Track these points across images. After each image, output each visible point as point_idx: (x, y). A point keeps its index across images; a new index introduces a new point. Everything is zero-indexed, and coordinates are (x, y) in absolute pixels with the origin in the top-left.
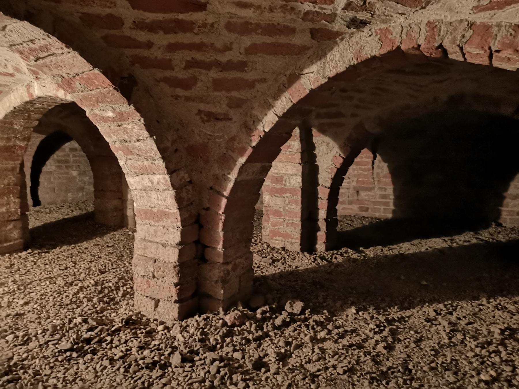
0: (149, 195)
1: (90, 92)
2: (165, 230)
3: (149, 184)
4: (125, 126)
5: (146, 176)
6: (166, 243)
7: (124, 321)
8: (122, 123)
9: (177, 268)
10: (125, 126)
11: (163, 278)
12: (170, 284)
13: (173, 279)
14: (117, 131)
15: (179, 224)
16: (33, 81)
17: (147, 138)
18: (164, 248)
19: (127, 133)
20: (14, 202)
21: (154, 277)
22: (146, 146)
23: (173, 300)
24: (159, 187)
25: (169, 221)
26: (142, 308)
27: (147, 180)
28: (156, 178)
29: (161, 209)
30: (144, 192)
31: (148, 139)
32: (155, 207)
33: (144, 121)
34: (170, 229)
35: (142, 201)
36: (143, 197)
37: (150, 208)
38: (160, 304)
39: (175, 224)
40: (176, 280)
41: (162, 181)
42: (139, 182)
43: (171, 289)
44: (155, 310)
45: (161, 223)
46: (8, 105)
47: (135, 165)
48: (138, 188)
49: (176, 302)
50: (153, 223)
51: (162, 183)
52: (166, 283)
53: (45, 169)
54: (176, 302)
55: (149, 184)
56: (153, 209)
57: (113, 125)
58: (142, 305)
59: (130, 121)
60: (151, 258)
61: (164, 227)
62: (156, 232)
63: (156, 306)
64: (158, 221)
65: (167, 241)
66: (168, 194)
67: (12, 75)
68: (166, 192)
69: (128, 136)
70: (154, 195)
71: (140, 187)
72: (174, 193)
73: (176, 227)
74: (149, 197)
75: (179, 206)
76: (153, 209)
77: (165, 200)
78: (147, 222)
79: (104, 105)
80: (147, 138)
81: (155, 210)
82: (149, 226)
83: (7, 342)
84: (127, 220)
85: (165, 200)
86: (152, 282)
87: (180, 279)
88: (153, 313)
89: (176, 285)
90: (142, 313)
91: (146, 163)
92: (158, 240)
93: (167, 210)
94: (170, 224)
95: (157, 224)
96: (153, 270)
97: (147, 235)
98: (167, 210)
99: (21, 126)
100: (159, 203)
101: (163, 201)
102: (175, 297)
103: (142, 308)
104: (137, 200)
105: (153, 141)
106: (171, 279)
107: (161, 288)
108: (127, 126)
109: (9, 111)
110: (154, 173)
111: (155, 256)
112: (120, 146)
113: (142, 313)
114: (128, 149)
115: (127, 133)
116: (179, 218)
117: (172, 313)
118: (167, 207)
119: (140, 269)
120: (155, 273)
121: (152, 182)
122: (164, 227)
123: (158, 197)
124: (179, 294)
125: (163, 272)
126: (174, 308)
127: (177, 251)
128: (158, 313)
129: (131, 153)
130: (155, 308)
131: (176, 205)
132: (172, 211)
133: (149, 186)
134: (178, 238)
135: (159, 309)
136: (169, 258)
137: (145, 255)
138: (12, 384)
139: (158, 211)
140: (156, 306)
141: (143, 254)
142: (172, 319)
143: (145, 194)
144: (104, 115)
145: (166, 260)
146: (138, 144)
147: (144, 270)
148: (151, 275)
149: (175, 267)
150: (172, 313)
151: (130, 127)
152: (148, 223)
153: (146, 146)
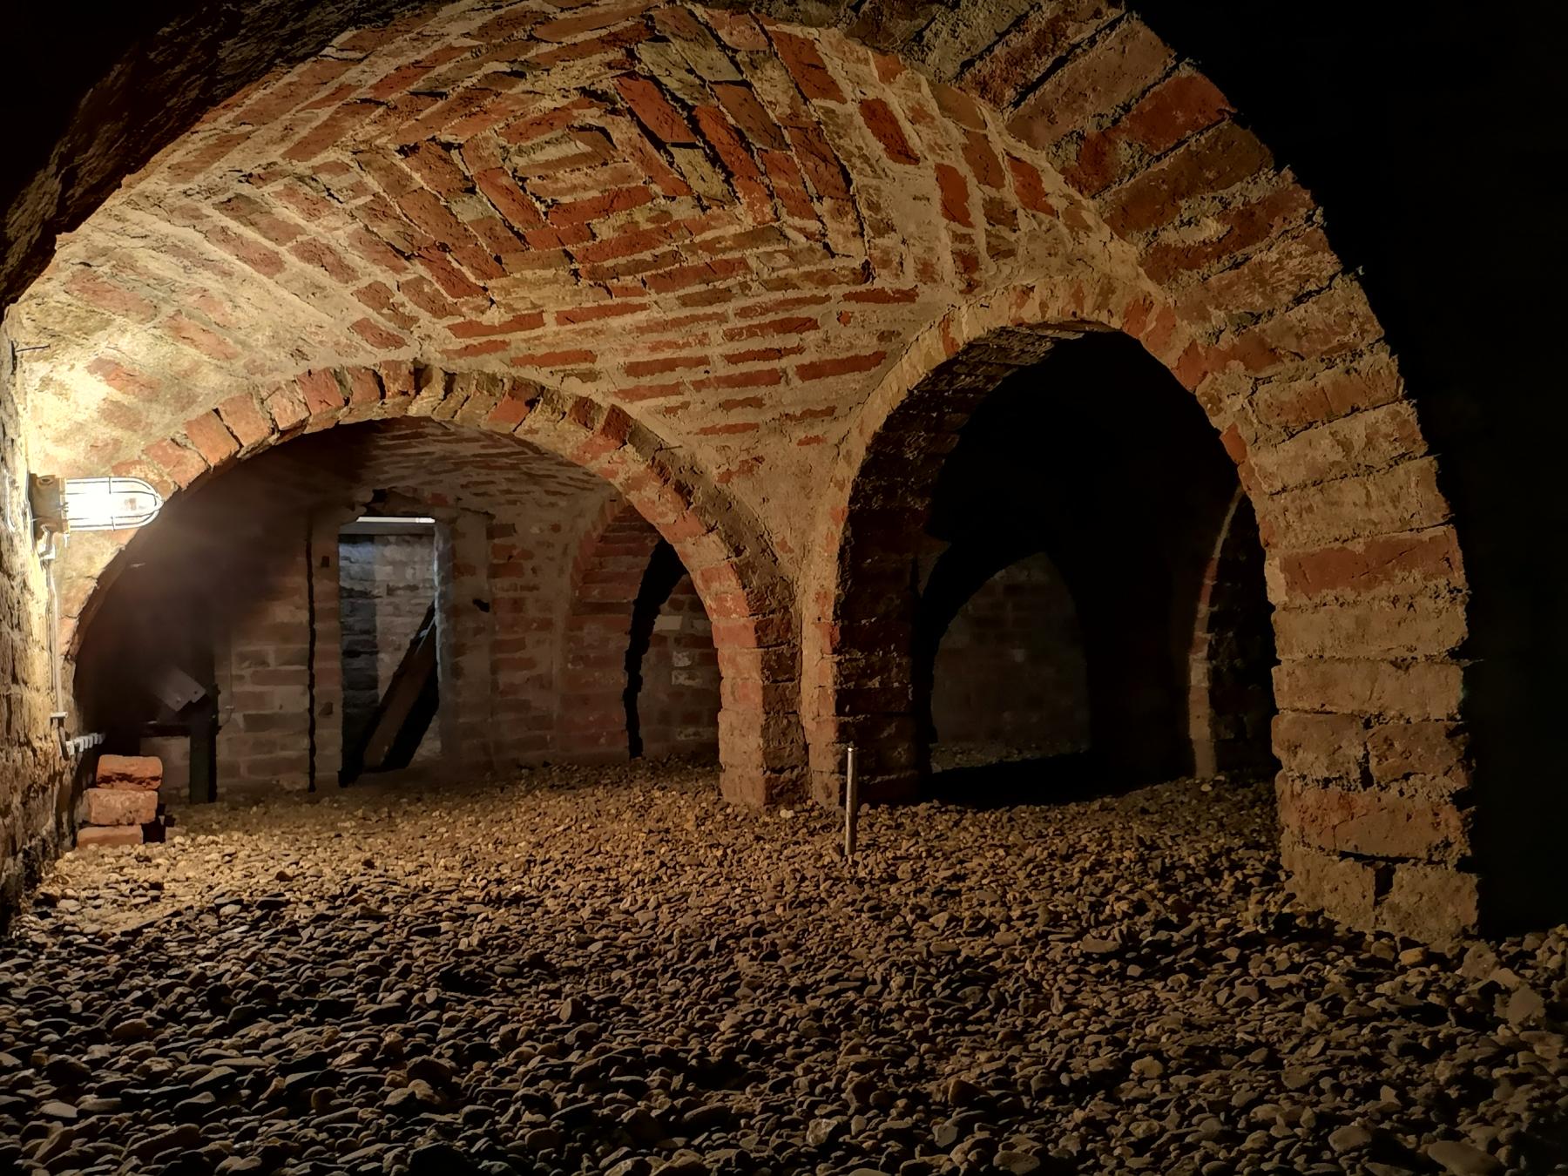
0: (1335, 496)
1: (1155, 168)
2: (1401, 609)
3: (1337, 455)
4: (1256, 258)
5: (1325, 430)
6: (1409, 655)
7: (1271, 920)
8: (1248, 250)
9: (1460, 738)
10: (1256, 258)
11: (1406, 777)
12: (1434, 797)
13: (1446, 780)
14: (1230, 286)
15: (1459, 577)
16: (959, 301)
17: (1332, 278)
18: (1401, 672)
19: (1263, 283)
20: (899, 665)
21: (1367, 780)
22: (1329, 310)
23: (1452, 860)
24: (1375, 458)
25: (1417, 573)
26: (1328, 897)
27: (1326, 442)
28: (1356, 428)
29: (1381, 539)
30: (1312, 490)
31: (1338, 280)
32: (1356, 536)
33: (1325, 216)
34: (1424, 602)
35: (1308, 527)
36: (1310, 509)
37: (1337, 545)
38: (1401, 874)
39: (1442, 582)
40: (1458, 782)
41: (1384, 429)
42: (1296, 457)
43: (1442, 816)
44: (1377, 903)
45: (1383, 589)
46: (895, 389)
47: (1285, 397)
48: (1291, 483)
49: (1463, 865)
50: (1350, 595)
51: (1387, 436)
52: (1420, 799)
53: (946, 642)
54: (1463, 865)
55: (1337, 455)
56: (1349, 545)
57: (1217, 267)
58: (1327, 888)
59: (1274, 233)
60: (1352, 717)
61: (1395, 601)
62: (1362, 623)
63: (1384, 884)
64: (1369, 586)
65: (1410, 650)
66: (1407, 473)
67: (909, 296)
68: (1400, 470)
69: (1263, 294)
70: (1352, 492)
71: (1300, 474)
72: (1435, 463)
73: (1444, 592)
74: (1333, 504)
75: (1452, 508)
76: (1349, 545)
77: (1395, 500)
78: (1329, 595)
79: (1193, 202)
80: (1332, 278)
81: (1358, 547)
82: (1336, 607)
83: (933, 927)
84: (1192, 754)
85: (1395, 500)
86: (1363, 798)
87: (1475, 778)
88: (1372, 915)
89: (1459, 800)
90: (1326, 914)
91: (1325, 378)
92: (1374, 650)
93: (1407, 535)
94: (1420, 585)
95: (1366, 596)
96: (1362, 753)
97: (1329, 643)
98: (1407, 535)
99: (921, 450)
100: (1374, 516)
101: (1389, 506)
102: (1461, 848)
103: (1328, 897)
104: (1288, 526)
105: (1356, 284)
106: (1441, 780)
107: (1402, 817)
108: (1264, 256)
109: (896, 404)
110: (1355, 410)
111: (1366, 707)
112: (1236, 341)
113: (1326, 914)
114: (1261, 342)
115: (1263, 283)
116: (1458, 556)
117: (1451, 909)
118: (1405, 524)
119: (1311, 757)
120: (1373, 763)
121: (1346, 446)
122: (1395, 601)
123: (1368, 494)
124: (1475, 833)
125: (1406, 754)
126: (1458, 889)
127: (1455, 675)
128: (1394, 909)
129: (1273, 355)
130: (1377, 894)
131: (1440, 506)
132: (1425, 536)
133: (1334, 464)
134: (1456, 627)
135: (1395, 896)
136: (1423, 706)
137: (1328, 708)
138: (976, 988)
139: (1368, 547)
140: (1384, 884)
141: (1317, 707)
142: (1453, 927)
143: (1318, 497)
144: (1190, 242)
145: (1414, 715)
146: (1300, 311)
147: (1324, 760)
148: (1356, 774)
149: (1451, 734)
150: (1451, 909)
151: (1273, 256)
152: (1330, 598)
153: (1329, 310)
